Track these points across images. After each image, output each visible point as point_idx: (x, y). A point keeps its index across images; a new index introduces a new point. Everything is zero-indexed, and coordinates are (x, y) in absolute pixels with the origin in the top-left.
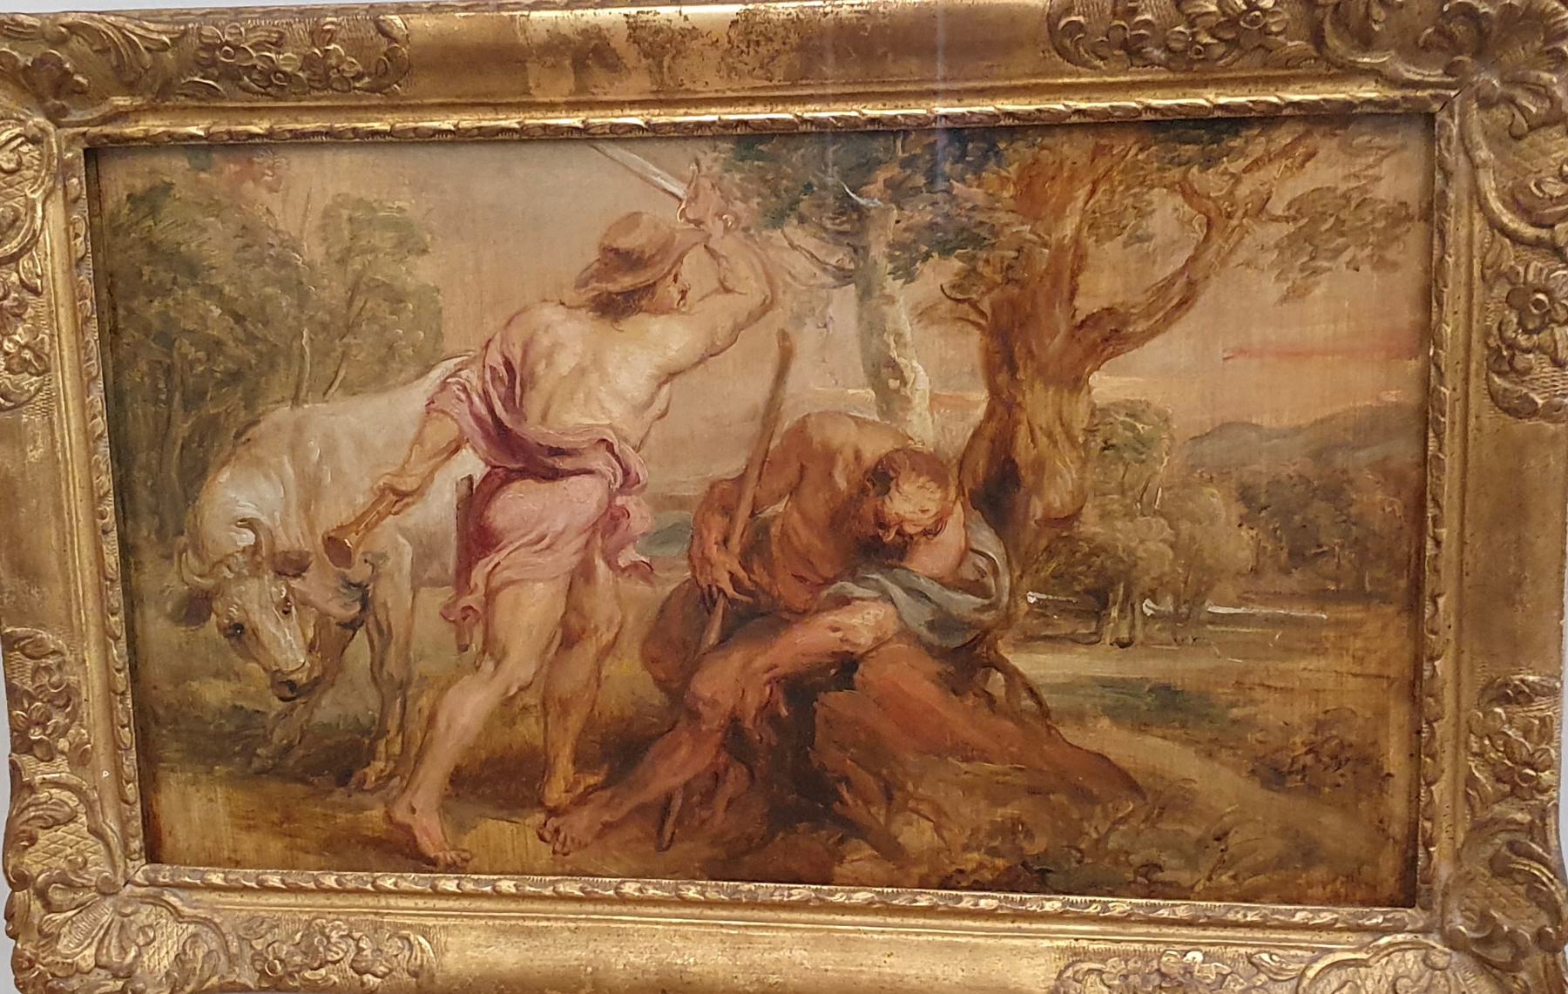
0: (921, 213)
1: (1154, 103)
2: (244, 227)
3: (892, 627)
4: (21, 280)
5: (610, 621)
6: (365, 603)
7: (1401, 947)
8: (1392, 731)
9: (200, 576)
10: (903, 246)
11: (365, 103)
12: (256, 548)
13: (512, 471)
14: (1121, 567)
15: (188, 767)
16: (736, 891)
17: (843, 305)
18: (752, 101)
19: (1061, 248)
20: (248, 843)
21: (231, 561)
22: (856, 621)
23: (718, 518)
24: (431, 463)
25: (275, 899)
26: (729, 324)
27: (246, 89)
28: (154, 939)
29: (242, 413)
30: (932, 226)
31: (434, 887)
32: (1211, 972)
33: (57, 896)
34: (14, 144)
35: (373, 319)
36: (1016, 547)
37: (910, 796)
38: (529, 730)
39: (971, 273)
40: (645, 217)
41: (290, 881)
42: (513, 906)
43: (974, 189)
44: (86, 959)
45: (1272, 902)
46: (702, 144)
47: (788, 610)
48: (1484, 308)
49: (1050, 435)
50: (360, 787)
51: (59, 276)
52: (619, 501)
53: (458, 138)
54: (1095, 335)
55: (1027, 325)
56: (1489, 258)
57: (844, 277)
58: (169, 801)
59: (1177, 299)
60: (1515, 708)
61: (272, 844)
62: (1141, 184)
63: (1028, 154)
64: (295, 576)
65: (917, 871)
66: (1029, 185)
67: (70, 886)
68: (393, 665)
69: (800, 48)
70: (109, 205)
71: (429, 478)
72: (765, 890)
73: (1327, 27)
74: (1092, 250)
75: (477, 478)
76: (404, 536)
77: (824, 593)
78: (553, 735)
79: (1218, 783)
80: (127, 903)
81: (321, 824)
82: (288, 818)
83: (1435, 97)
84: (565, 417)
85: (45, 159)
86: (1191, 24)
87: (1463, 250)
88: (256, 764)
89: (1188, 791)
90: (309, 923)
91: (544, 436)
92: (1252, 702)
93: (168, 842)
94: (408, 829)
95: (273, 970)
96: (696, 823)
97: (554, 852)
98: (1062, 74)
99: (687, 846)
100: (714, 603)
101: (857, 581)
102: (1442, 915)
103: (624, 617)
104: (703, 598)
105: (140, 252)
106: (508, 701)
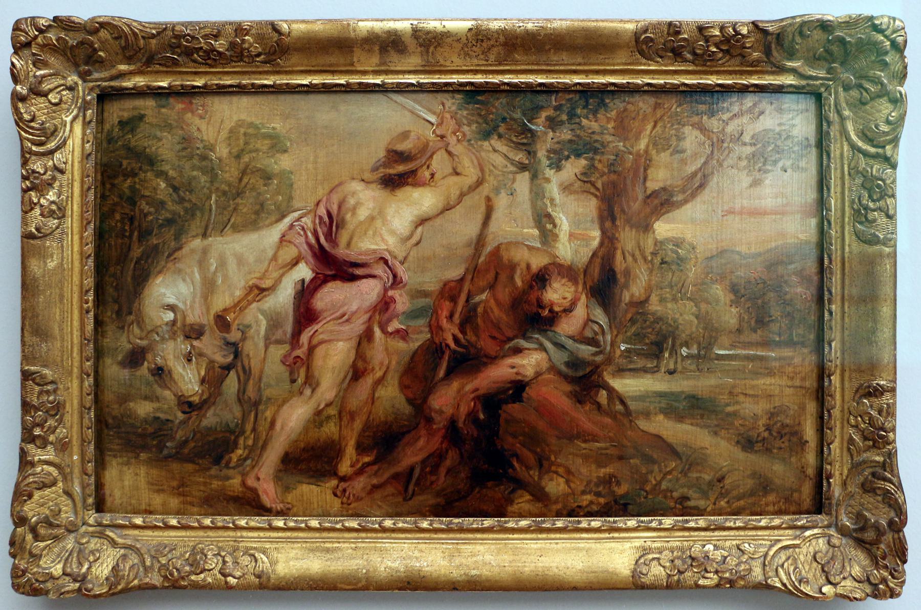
0: (565, 134)
1: (686, 82)
2: (184, 138)
3: (545, 365)
4: (54, 165)
5: (382, 364)
6: (237, 354)
7: (816, 537)
8: (809, 417)
9: (141, 339)
10: (554, 152)
11: (260, 69)
12: (174, 322)
13: (329, 276)
14: (670, 329)
15: (124, 454)
16: (451, 522)
17: (523, 182)
18: (476, 72)
19: (638, 155)
20: (157, 500)
21: (160, 330)
22: (525, 362)
23: (447, 303)
24: (281, 271)
25: (173, 533)
26: (458, 193)
27: (195, 61)
28: (98, 559)
29: (173, 243)
30: (570, 141)
31: (270, 525)
32: (718, 555)
33: (42, 531)
34: (58, 90)
35: (253, 189)
36: (615, 318)
37: (552, 464)
38: (331, 429)
39: (592, 167)
40: (412, 134)
41: (183, 522)
42: (317, 535)
43: (593, 123)
44: (57, 570)
45: (748, 515)
46: (446, 95)
47: (486, 356)
48: (850, 190)
49: (633, 256)
50: (227, 466)
51: (76, 165)
52: (390, 293)
53: (311, 89)
54: (656, 202)
55: (619, 198)
56: (852, 165)
57: (523, 168)
58: (111, 474)
59: (696, 185)
60: (872, 399)
61: (172, 500)
62: (679, 123)
63: (622, 106)
64: (196, 339)
65: (555, 507)
66: (622, 122)
67: (51, 525)
68: (251, 392)
69: (505, 44)
70: (107, 126)
71: (278, 281)
72: (467, 521)
73: (773, 46)
74: (654, 157)
75: (307, 280)
76: (262, 314)
77: (507, 346)
78: (344, 432)
79: (720, 450)
80: (83, 536)
81: (202, 488)
82: (182, 485)
83: (822, 84)
84: (364, 245)
85: (75, 100)
86: (707, 41)
87: (838, 161)
88: (165, 452)
89: (704, 454)
90: (194, 547)
91: (348, 255)
92: (737, 403)
93: (109, 500)
94: (254, 491)
95: (172, 575)
96: (428, 483)
97: (342, 503)
98: (641, 64)
99: (421, 498)
100: (443, 353)
101: (524, 337)
102: (836, 517)
103: (390, 362)
104: (433, 350)
105: (123, 152)
106: (318, 413)
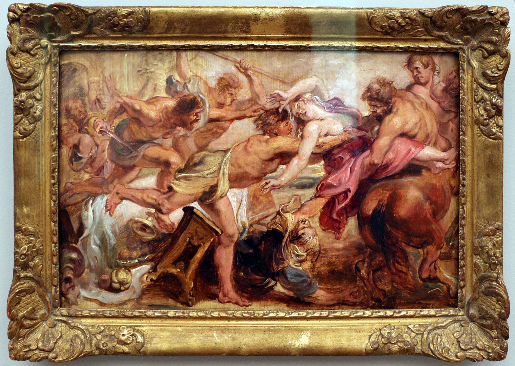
83: (460, 48)
